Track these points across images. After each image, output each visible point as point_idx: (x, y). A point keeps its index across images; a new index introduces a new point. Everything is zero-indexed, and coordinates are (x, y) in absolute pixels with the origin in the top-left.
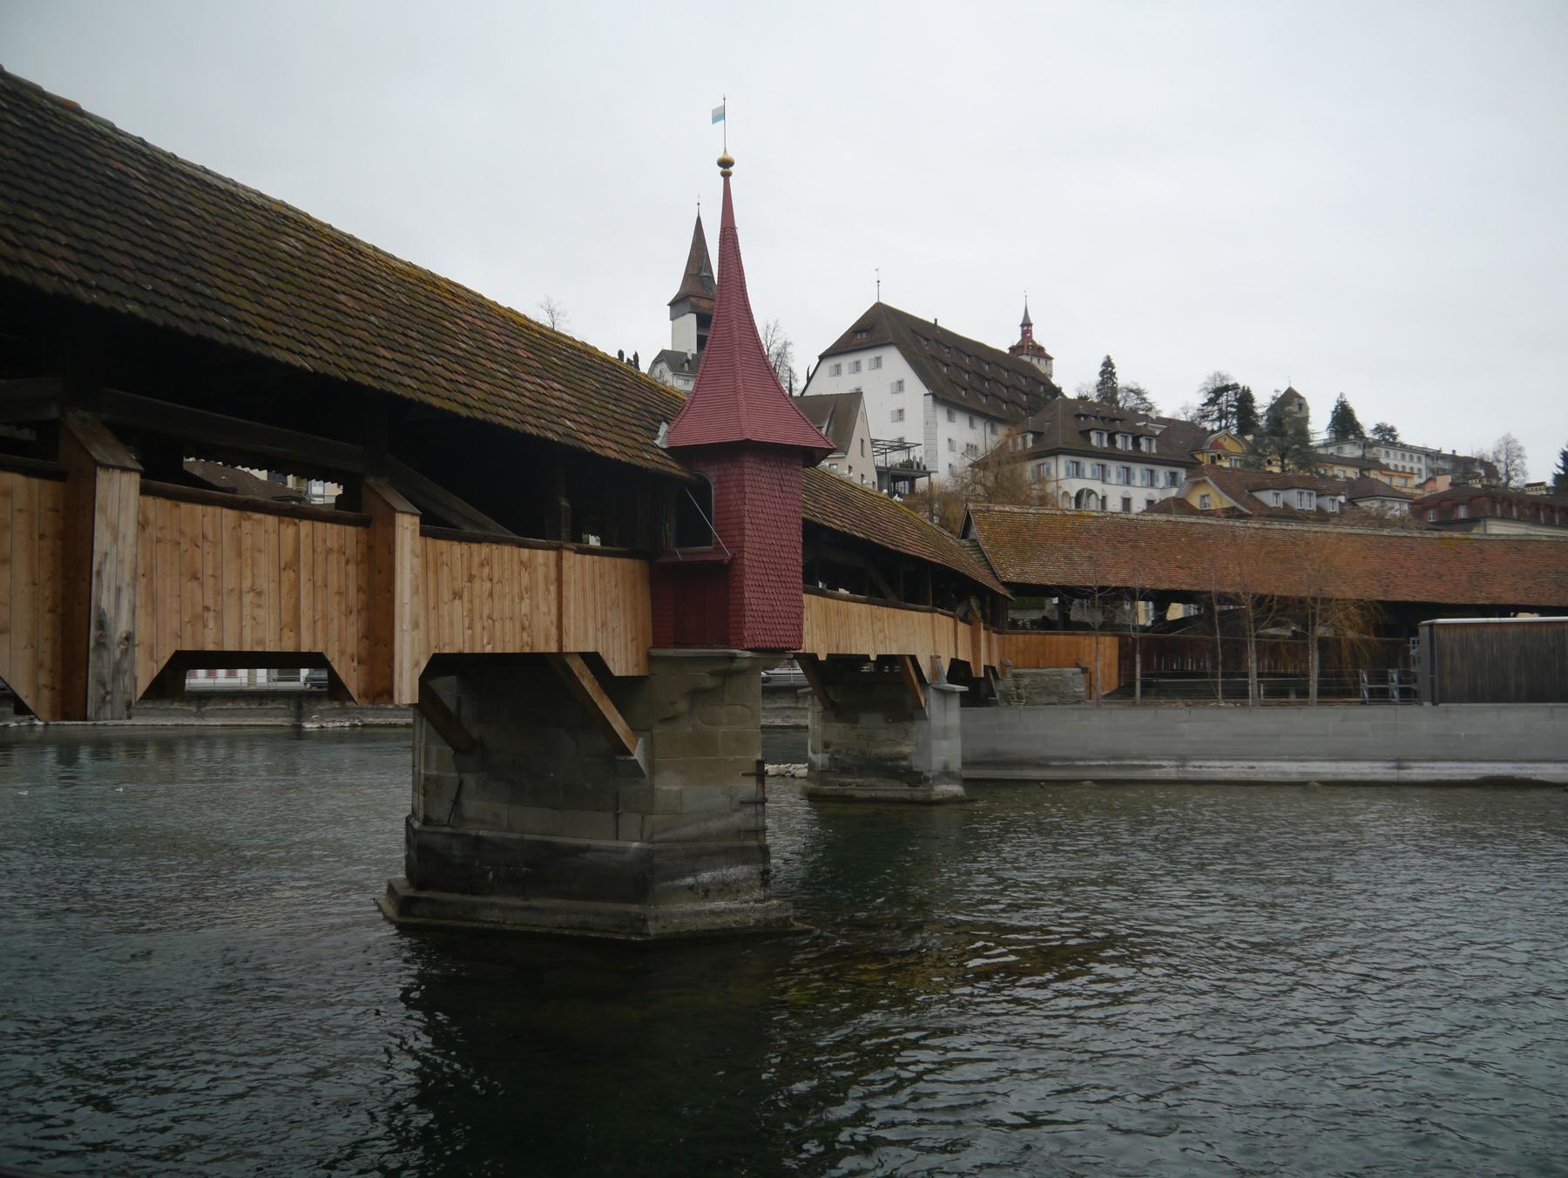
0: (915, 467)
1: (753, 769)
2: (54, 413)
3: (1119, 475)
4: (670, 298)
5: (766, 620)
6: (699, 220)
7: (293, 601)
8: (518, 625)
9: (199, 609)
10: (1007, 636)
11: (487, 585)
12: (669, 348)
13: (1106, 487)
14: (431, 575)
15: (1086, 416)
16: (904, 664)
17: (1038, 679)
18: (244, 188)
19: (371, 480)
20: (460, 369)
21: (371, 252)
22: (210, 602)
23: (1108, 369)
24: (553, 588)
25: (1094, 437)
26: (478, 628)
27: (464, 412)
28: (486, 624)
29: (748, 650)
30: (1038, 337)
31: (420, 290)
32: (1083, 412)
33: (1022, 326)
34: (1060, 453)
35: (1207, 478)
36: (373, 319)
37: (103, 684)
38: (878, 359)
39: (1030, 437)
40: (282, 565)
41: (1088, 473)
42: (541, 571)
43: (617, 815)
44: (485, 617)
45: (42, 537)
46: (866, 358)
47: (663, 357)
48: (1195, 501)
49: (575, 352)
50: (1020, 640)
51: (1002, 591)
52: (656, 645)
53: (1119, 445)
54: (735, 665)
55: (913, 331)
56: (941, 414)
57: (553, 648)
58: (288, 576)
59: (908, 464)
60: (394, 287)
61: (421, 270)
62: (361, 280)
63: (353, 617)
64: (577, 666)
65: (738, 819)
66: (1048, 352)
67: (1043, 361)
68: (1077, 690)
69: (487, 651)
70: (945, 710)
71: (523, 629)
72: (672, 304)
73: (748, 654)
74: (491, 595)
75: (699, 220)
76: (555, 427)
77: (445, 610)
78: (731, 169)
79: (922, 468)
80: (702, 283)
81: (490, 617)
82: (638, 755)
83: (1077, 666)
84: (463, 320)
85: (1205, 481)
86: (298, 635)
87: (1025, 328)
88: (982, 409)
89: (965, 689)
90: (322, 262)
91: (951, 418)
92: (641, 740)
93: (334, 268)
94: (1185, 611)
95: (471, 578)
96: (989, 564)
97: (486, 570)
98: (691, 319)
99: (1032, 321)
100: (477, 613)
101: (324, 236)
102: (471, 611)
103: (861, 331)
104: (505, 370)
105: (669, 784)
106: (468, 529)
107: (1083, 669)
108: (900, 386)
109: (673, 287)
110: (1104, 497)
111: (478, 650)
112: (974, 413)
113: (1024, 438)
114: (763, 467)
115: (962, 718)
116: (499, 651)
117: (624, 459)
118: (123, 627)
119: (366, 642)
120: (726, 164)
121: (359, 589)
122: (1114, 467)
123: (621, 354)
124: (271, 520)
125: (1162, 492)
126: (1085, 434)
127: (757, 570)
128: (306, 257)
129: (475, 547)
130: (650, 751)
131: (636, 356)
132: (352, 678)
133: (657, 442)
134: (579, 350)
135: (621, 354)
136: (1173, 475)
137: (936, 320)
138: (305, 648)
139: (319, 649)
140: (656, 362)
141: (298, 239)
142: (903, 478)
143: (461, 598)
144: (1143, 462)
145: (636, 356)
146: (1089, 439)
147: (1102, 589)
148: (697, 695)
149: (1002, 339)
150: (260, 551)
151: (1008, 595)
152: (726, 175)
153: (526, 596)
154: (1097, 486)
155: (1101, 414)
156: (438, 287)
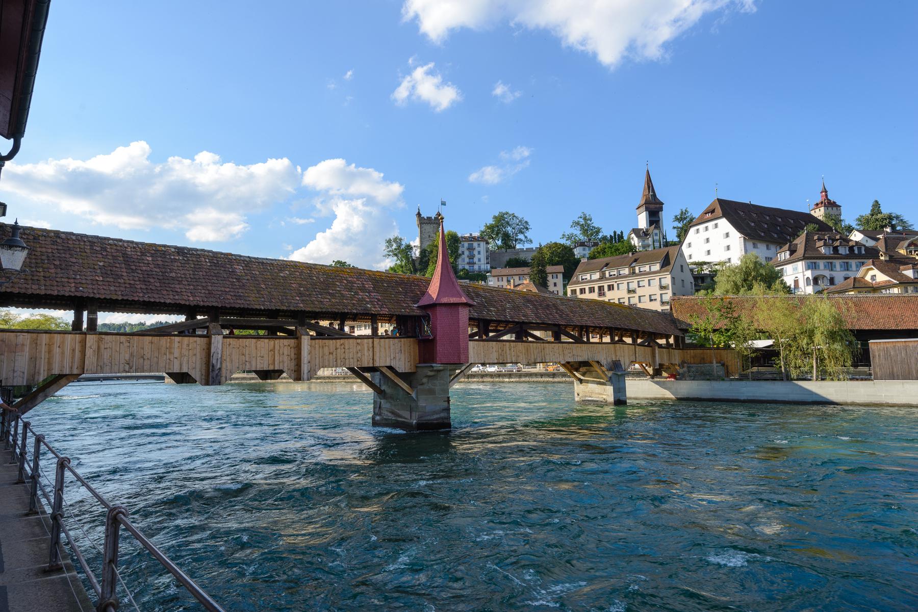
2: (208, 324)
8: (355, 360)
13: (832, 272)
14: (321, 349)
22: (247, 360)
23: (876, 205)
24: (371, 350)
30: (832, 198)
37: (213, 378)
41: (822, 266)
45: (204, 349)
46: (710, 225)
65: (442, 415)
67: (835, 209)
71: (358, 361)
82: (414, 395)
91: (755, 246)
97: (343, 346)
100: (338, 358)
105: (422, 403)
108: (727, 235)
118: (219, 366)
121: (295, 354)
123: (615, 233)
129: (338, 341)
131: (622, 232)
135: (615, 233)
138: (276, 369)
139: (281, 369)
144: (823, 259)
145: (622, 232)
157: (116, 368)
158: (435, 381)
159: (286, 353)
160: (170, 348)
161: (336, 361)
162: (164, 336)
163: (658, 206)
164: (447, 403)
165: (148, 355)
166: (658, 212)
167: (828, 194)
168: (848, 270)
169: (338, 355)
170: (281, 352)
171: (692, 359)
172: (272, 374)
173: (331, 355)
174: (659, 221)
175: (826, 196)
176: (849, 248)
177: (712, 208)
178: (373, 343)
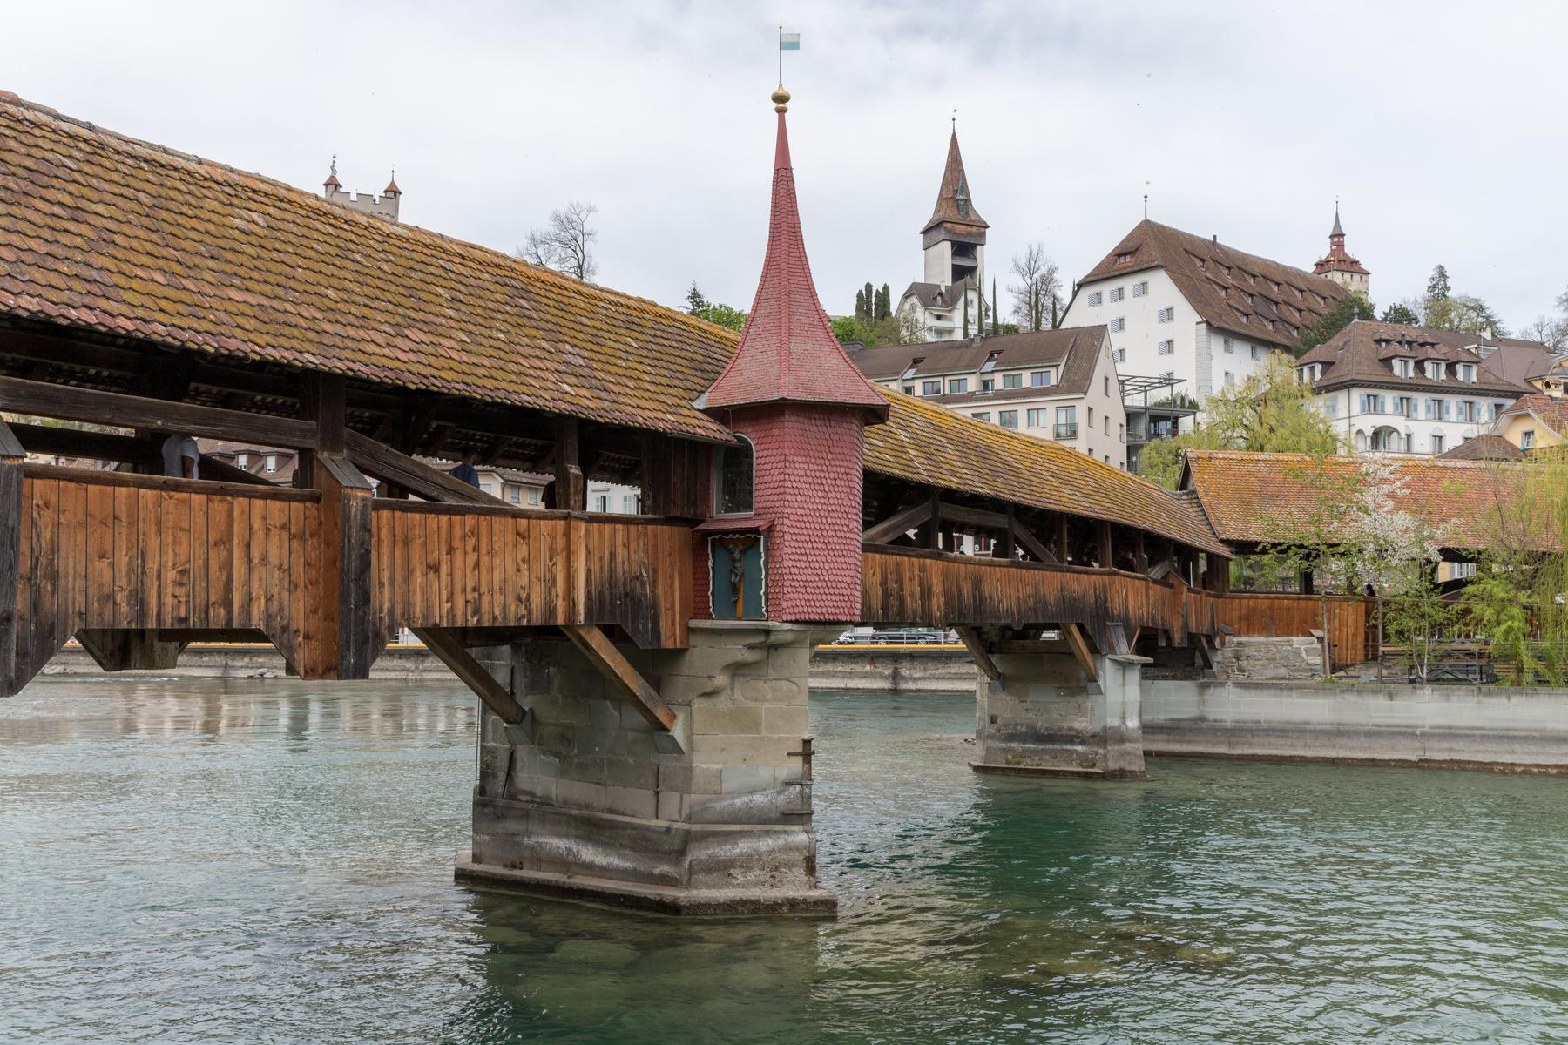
1: (800, 749)
3: (1428, 409)
4: (923, 225)
6: (954, 137)
11: (472, 558)
13: (1410, 423)
15: (1388, 342)
19: (324, 456)
25: (1397, 365)
26: (459, 601)
28: (470, 597)
29: (787, 621)
30: (1351, 250)
32: (1385, 336)
34: (1354, 386)
35: (1530, 411)
38: (1144, 284)
39: (1318, 368)
40: (212, 541)
41: (1389, 408)
42: (544, 543)
43: (657, 793)
44: (468, 589)
46: (1129, 284)
47: (914, 290)
48: (1515, 437)
49: (621, 309)
51: (1224, 551)
53: (1429, 374)
54: (773, 638)
56: (1217, 343)
59: (1171, 403)
63: (300, 593)
66: (1364, 266)
67: (1357, 277)
70: (1124, 685)
71: (519, 599)
72: (924, 232)
73: (787, 626)
75: (954, 137)
79: (1187, 404)
85: (1528, 415)
87: (1336, 240)
91: (1228, 349)
94: (1452, 572)
95: (450, 551)
98: (946, 248)
100: (458, 588)
106: (450, 501)
108: (1168, 314)
109: (927, 215)
110: (1409, 436)
112: (1259, 343)
113: (1312, 369)
120: (781, 99)
121: (307, 564)
122: (1421, 400)
123: (869, 287)
125: (1455, 433)
126: (1386, 362)
127: (799, 538)
129: (457, 519)
131: (886, 288)
135: (869, 287)
136: (1498, 407)
137: (1215, 237)
140: (906, 296)
142: (1166, 418)
145: (886, 288)
146: (1391, 369)
147: (1274, 545)
148: (737, 669)
152: (781, 112)
154: (1399, 423)
155: (1408, 338)
158: (760, 684)
159: (274, 559)
161: (450, 598)
163: (974, 230)
164: (800, 759)
166: (974, 246)
168: (1471, 420)
169: (458, 574)
170: (256, 555)
172: (157, 645)
175: (1340, 245)
176: (1448, 365)
177: (1133, 244)
178: (567, 534)
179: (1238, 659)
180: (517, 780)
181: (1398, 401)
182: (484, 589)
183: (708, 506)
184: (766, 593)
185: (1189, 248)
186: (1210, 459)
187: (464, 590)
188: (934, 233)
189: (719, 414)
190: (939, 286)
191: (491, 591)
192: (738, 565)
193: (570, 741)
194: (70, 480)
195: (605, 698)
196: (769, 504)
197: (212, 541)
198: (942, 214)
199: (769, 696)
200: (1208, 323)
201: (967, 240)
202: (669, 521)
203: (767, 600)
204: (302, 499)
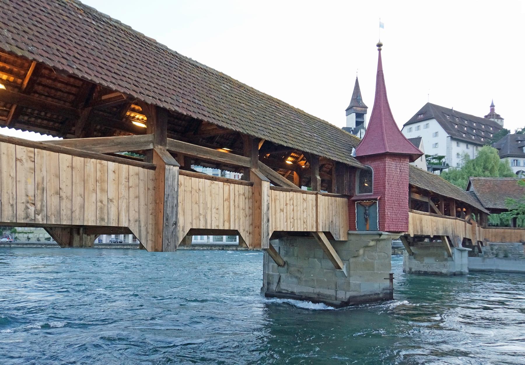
0: (443, 165)
1: (388, 277)
2: (151, 147)
5: (394, 220)
7: (228, 212)
9: (198, 214)
10: (487, 229)
11: (292, 207)
12: (345, 126)
16: (444, 239)
17: (502, 246)
18: (210, 68)
20: (283, 129)
21: (251, 89)
24: (314, 208)
26: (289, 222)
27: (285, 145)
28: (291, 221)
29: (387, 232)
30: (497, 112)
31: (268, 102)
32: (519, 139)
33: (491, 106)
36: (253, 112)
40: (225, 199)
46: (422, 124)
50: (493, 230)
51: (486, 211)
52: (350, 229)
54: (382, 237)
55: (442, 112)
56: (454, 144)
57: (314, 230)
58: (226, 203)
60: (260, 102)
61: (268, 95)
62: (249, 99)
63: (248, 218)
64: (323, 237)
66: (501, 117)
67: (499, 120)
68: (520, 252)
69: (292, 231)
71: (304, 222)
72: (347, 110)
73: (387, 233)
74: (293, 210)
76: (316, 149)
77: (278, 215)
78: (382, 47)
79: (446, 165)
80: (358, 102)
81: (293, 218)
83: (520, 242)
84: (283, 113)
86: (230, 224)
87: (492, 108)
88: (472, 141)
89: (471, 250)
90: (236, 93)
92: (345, 264)
93: (239, 95)
95: (286, 204)
96: (479, 201)
97: (292, 201)
98: (354, 115)
99: (495, 105)
101: (236, 84)
102: (287, 216)
103: (419, 115)
104: (298, 130)
105: (354, 281)
106: (285, 187)
107: (523, 243)
109: (347, 104)
111: (289, 230)
114: (393, 163)
115: (469, 261)
116: (296, 230)
117: (341, 161)
119: (251, 227)
120: (379, 45)
121: (249, 208)
124: (221, 184)
128: (230, 91)
129: (288, 193)
130: (348, 269)
132: (247, 240)
133: (352, 155)
134: (322, 123)
141: (227, 85)
143: (283, 211)
149: (481, 112)
150: (217, 194)
151: (489, 213)
152: (380, 50)
153: (305, 211)
156: (274, 101)
157: (375, 188)
158: (374, 253)
160: (102, 181)
161: (286, 222)
162: (91, 157)
163: (363, 109)
164: (388, 281)
165: (66, 192)
167: (495, 108)
171: (494, 237)
173: (282, 213)
174: (363, 122)
179: (492, 250)
180: (281, 285)
181: (513, 161)
182: (295, 218)
183: (354, 191)
184: (379, 221)
185: (443, 111)
186: (479, 180)
187: (290, 218)
188: (350, 110)
189: (360, 159)
190: (351, 128)
191: (297, 219)
192: (367, 212)
193: (301, 273)
194: (187, 176)
195: (315, 257)
196: (379, 190)
197: (225, 199)
198: (353, 104)
199: (377, 258)
200: (451, 137)
201: (361, 112)
202: (343, 196)
203: (379, 223)
204: (245, 184)
